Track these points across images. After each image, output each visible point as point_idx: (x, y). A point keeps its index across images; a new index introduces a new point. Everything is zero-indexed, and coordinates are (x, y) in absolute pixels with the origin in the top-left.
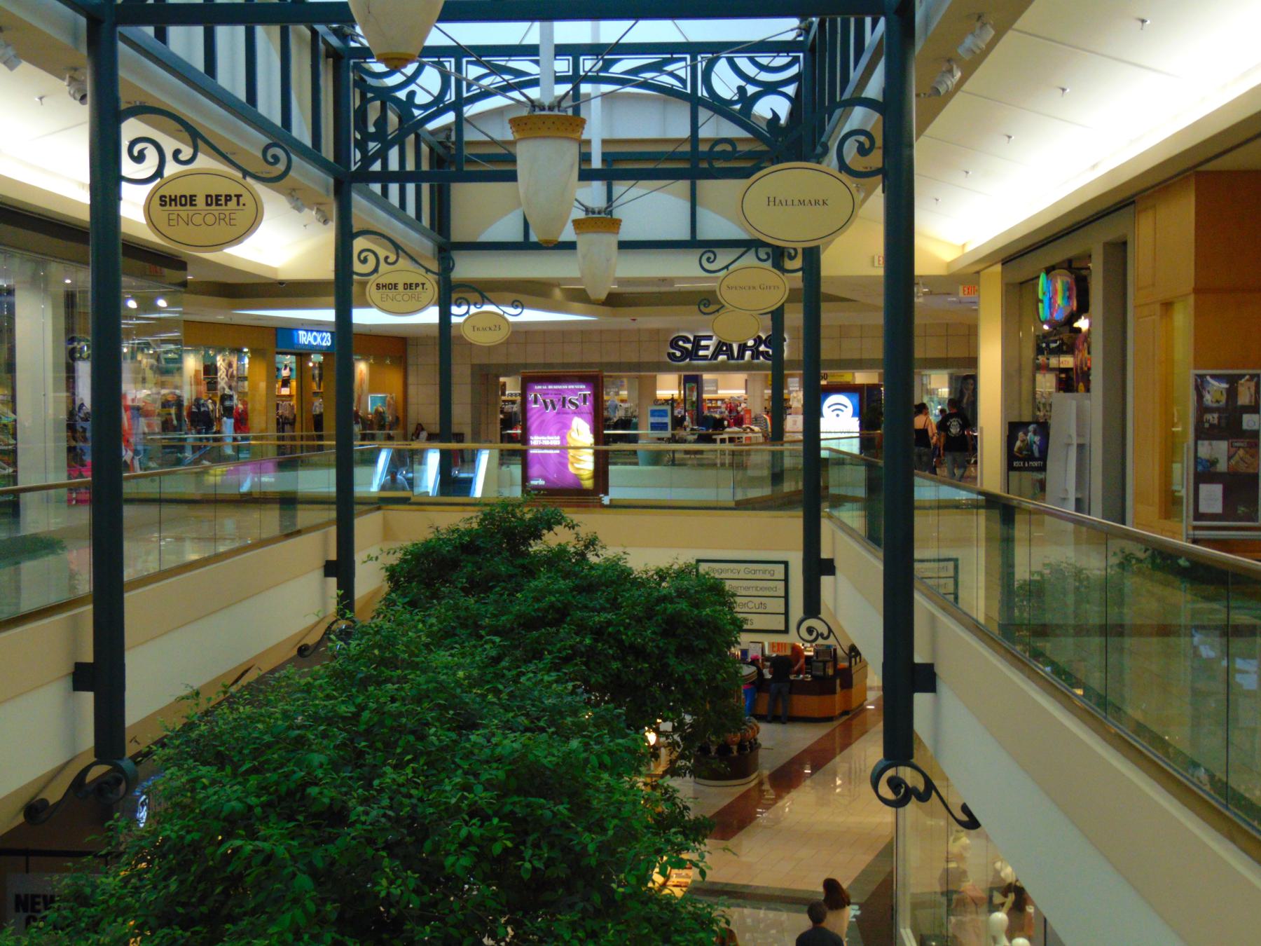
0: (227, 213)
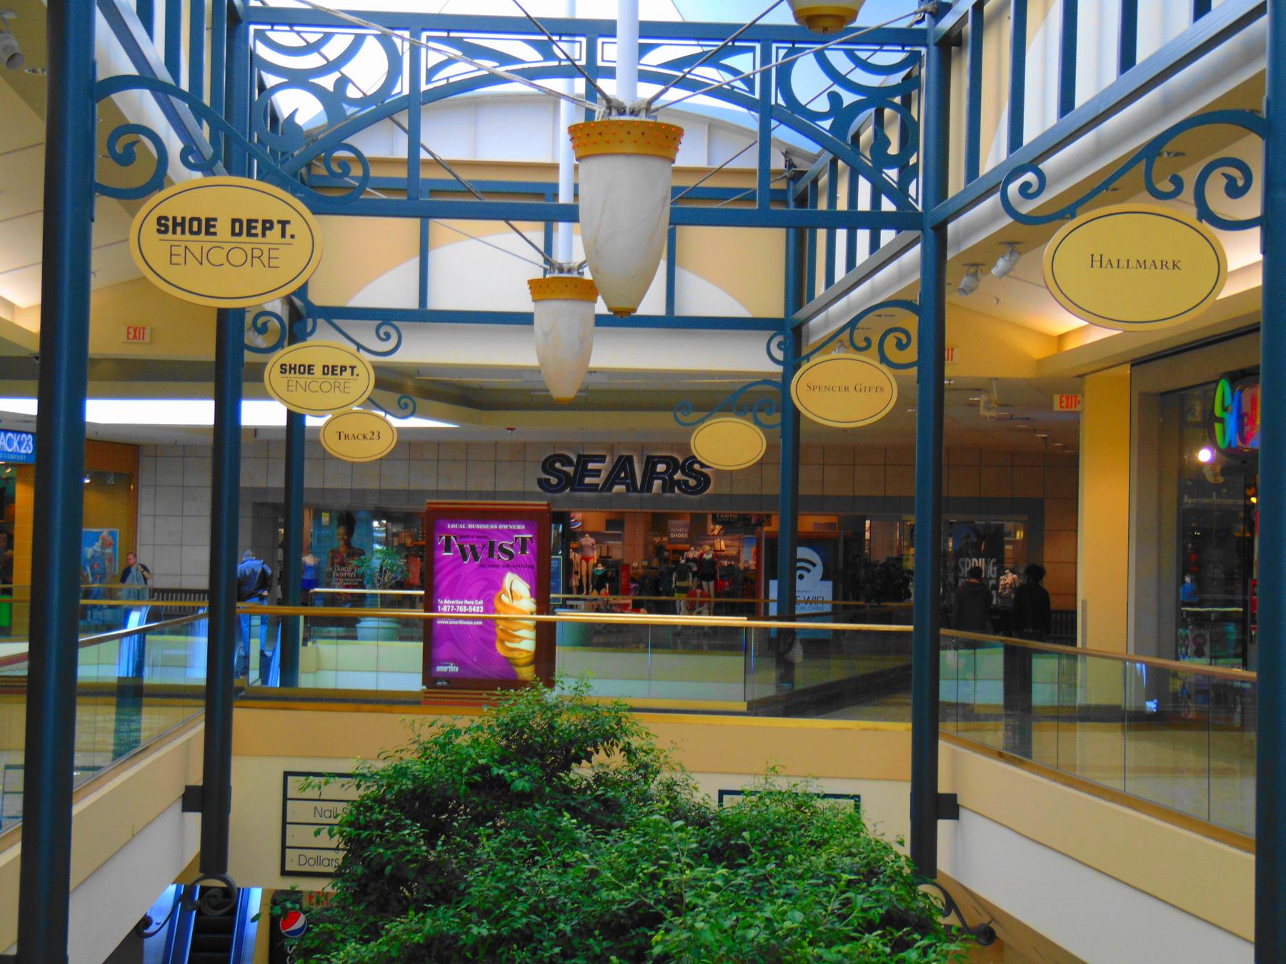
0: (265, 248)
